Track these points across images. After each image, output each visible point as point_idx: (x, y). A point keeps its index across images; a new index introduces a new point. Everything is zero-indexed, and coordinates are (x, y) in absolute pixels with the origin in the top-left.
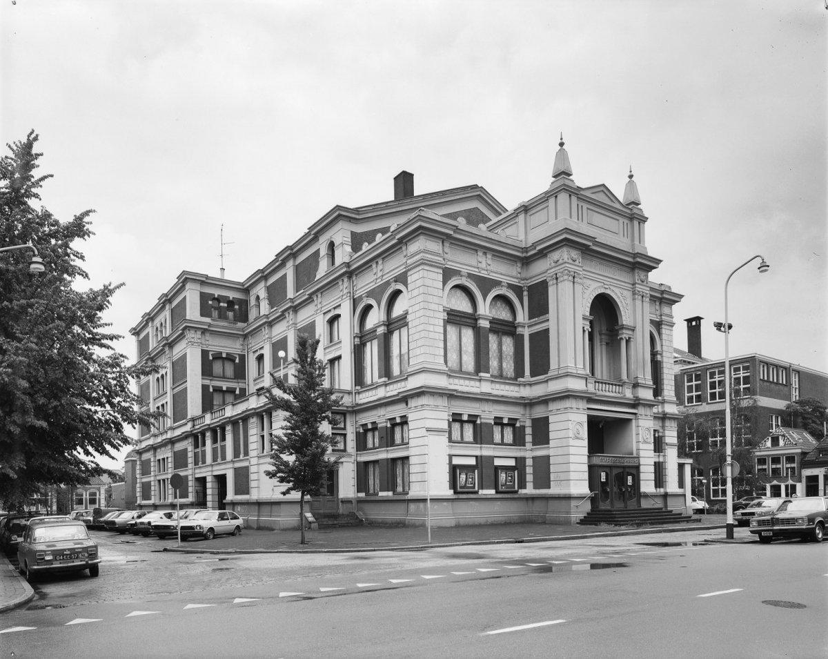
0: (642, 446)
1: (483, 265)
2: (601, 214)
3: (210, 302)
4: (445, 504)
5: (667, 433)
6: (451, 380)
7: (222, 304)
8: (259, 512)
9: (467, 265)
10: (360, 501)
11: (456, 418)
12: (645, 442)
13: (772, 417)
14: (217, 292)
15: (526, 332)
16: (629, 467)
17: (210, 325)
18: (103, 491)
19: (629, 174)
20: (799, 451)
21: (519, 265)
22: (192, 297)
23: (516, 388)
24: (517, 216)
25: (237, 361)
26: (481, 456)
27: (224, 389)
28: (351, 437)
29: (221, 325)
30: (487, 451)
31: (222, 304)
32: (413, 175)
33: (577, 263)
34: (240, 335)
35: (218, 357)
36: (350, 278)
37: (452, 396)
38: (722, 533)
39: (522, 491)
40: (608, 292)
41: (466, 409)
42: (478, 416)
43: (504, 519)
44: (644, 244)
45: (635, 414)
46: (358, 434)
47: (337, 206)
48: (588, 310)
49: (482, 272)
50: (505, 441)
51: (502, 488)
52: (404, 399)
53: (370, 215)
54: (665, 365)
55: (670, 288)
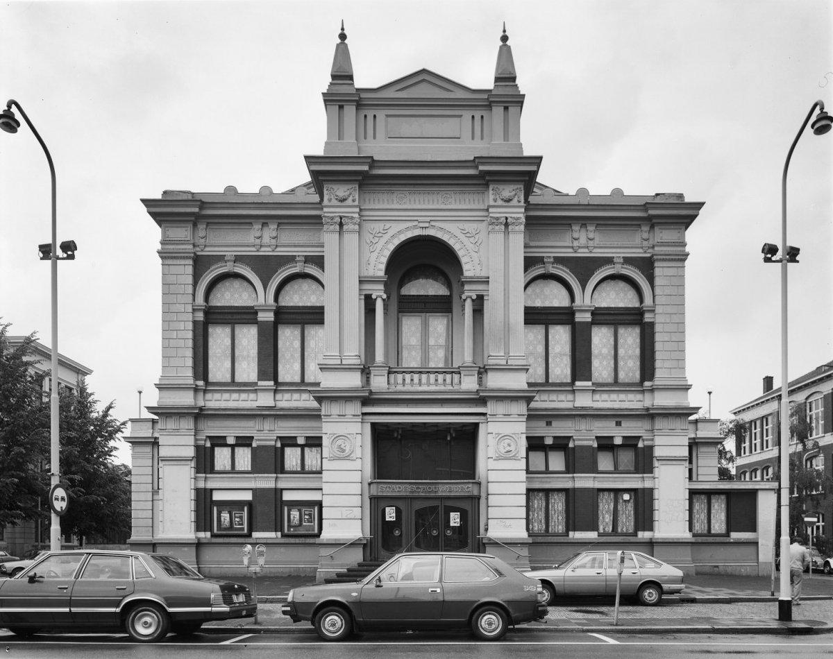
4: (186, 549)
5: (658, 440)
6: (597, 397)
9: (234, 246)
10: (199, 545)
11: (219, 441)
16: (449, 498)
21: (645, 228)
23: (639, 396)
33: (349, 202)
37: (200, 415)
38: (768, 615)
40: (431, 232)
41: (231, 431)
43: (287, 570)
45: (484, 414)
48: (383, 267)
50: (238, 468)
51: (288, 530)
54: (658, 328)
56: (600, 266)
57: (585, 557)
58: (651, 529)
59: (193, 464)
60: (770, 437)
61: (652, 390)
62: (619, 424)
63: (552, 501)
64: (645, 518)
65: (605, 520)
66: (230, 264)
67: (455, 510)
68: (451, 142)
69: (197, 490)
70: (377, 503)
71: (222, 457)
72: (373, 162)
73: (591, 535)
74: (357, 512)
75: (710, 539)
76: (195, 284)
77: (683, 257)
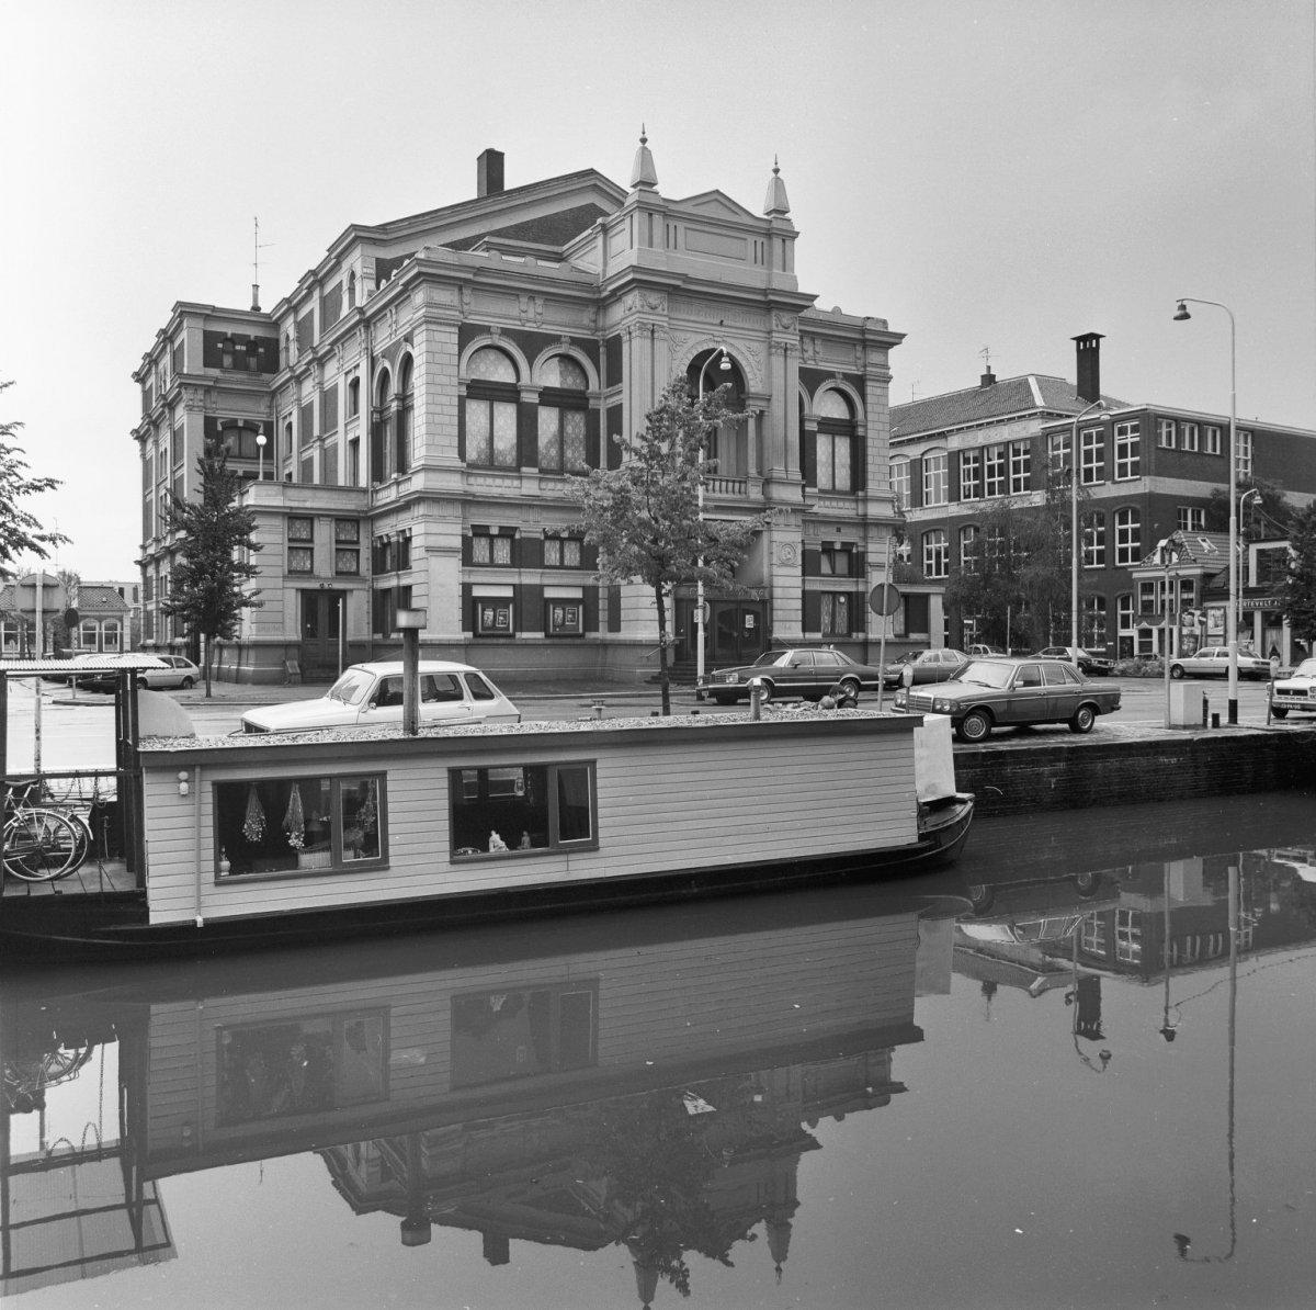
0: (776, 570)
1: (531, 315)
2: (708, 233)
3: (220, 345)
4: (454, 651)
5: (871, 547)
7: (238, 347)
11: (481, 531)
12: (784, 564)
13: (1186, 511)
14: (229, 330)
15: (603, 407)
17: (217, 380)
18: (127, 623)
20: (1198, 571)
21: (859, 348)
22: (190, 339)
24: (595, 238)
26: (521, 585)
27: (240, 473)
28: (365, 554)
29: (238, 379)
30: (530, 578)
31: (238, 347)
32: (502, 154)
34: (267, 392)
35: (231, 425)
36: (367, 327)
37: (467, 501)
39: (592, 635)
41: (495, 521)
42: (516, 528)
44: (792, 270)
46: (374, 549)
47: (352, 225)
48: (685, 369)
49: (528, 324)
51: (554, 630)
52: (406, 506)
53: (405, 232)
54: (870, 442)
55: (884, 322)
56: (823, 380)
57: (80, 658)
58: (863, 631)
59: (460, 556)
66: (496, 337)
71: (481, 550)
73: (818, 636)
76: (460, 355)
77: (887, 379)
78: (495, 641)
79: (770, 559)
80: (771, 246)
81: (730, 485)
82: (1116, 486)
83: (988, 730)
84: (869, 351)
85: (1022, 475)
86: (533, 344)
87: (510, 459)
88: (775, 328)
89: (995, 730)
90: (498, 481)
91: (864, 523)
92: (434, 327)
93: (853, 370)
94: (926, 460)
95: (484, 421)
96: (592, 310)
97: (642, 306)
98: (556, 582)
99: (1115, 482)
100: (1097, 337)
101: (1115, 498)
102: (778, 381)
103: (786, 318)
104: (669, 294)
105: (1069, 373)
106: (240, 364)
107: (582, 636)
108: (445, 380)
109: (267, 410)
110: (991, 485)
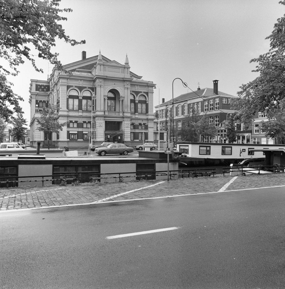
0: (125, 128)
1: (81, 83)
3: (39, 87)
5: (149, 124)
7: (42, 87)
8: (68, 144)
10: (68, 142)
11: (71, 122)
14: (40, 84)
17: (38, 93)
19: (126, 55)
21: (147, 87)
25: (46, 102)
30: (80, 130)
31: (42, 87)
33: (102, 82)
35: (41, 101)
36: (56, 85)
37: (68, 116)
50: (74, 127)
54: (149, 104)
58: (148, 140)
60: (164, 115)
61: (148, 115)
62: (142, 121)
63: (74, 124)
64: (146, 138)
65: (140, 138)
67: (119, 136)
68: (119, 74)
69: (67, 131)
70: (106, 135)
71: (71, 125)
72: (107, 77)
73: (138, 140)
74: (103, 136)
75: (156, 141)
77: (153, 93)
78: (73, 141)
79: (124, 126)
80: (125, 70)
81: (111, 113)
82: (215, 111)
83: (105, 154)
84: (149, 88)
85: (217, 106)
86: (81, 89)
87: (77, 109)
88: (125, 85)
89: (106, 154)
90: (74, 113)
91: (147, 120)
92: (62, 86)
93: (146, 91)
94: (178, 107)
95: (72, 102)
96: (93, 82)
97: (99, 82)
98: (85, 130)
99: (215, 110)
100: (217, 81)
101: (215, 114)
102: (126, 94)
103: (128, 83)
104: (104, 79)
105: (212, 87)
106: (43, 90)
107: (77, 140)
108: (64, 95)
109: (47, 99)
110: (216, 107)
